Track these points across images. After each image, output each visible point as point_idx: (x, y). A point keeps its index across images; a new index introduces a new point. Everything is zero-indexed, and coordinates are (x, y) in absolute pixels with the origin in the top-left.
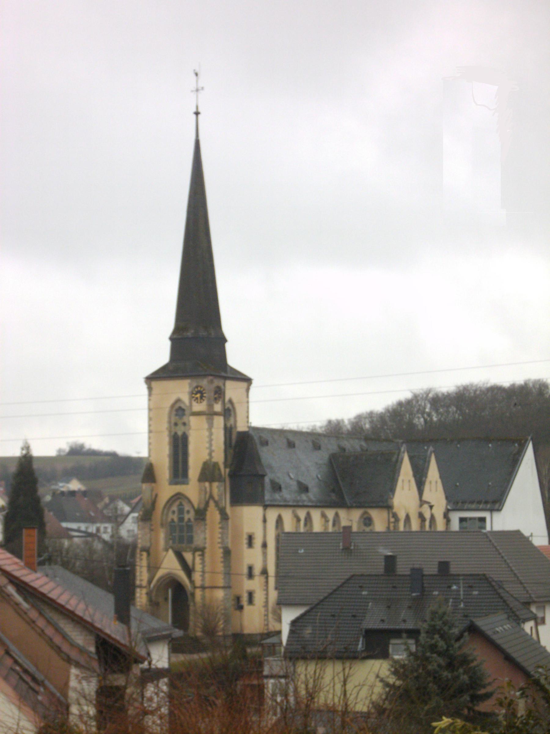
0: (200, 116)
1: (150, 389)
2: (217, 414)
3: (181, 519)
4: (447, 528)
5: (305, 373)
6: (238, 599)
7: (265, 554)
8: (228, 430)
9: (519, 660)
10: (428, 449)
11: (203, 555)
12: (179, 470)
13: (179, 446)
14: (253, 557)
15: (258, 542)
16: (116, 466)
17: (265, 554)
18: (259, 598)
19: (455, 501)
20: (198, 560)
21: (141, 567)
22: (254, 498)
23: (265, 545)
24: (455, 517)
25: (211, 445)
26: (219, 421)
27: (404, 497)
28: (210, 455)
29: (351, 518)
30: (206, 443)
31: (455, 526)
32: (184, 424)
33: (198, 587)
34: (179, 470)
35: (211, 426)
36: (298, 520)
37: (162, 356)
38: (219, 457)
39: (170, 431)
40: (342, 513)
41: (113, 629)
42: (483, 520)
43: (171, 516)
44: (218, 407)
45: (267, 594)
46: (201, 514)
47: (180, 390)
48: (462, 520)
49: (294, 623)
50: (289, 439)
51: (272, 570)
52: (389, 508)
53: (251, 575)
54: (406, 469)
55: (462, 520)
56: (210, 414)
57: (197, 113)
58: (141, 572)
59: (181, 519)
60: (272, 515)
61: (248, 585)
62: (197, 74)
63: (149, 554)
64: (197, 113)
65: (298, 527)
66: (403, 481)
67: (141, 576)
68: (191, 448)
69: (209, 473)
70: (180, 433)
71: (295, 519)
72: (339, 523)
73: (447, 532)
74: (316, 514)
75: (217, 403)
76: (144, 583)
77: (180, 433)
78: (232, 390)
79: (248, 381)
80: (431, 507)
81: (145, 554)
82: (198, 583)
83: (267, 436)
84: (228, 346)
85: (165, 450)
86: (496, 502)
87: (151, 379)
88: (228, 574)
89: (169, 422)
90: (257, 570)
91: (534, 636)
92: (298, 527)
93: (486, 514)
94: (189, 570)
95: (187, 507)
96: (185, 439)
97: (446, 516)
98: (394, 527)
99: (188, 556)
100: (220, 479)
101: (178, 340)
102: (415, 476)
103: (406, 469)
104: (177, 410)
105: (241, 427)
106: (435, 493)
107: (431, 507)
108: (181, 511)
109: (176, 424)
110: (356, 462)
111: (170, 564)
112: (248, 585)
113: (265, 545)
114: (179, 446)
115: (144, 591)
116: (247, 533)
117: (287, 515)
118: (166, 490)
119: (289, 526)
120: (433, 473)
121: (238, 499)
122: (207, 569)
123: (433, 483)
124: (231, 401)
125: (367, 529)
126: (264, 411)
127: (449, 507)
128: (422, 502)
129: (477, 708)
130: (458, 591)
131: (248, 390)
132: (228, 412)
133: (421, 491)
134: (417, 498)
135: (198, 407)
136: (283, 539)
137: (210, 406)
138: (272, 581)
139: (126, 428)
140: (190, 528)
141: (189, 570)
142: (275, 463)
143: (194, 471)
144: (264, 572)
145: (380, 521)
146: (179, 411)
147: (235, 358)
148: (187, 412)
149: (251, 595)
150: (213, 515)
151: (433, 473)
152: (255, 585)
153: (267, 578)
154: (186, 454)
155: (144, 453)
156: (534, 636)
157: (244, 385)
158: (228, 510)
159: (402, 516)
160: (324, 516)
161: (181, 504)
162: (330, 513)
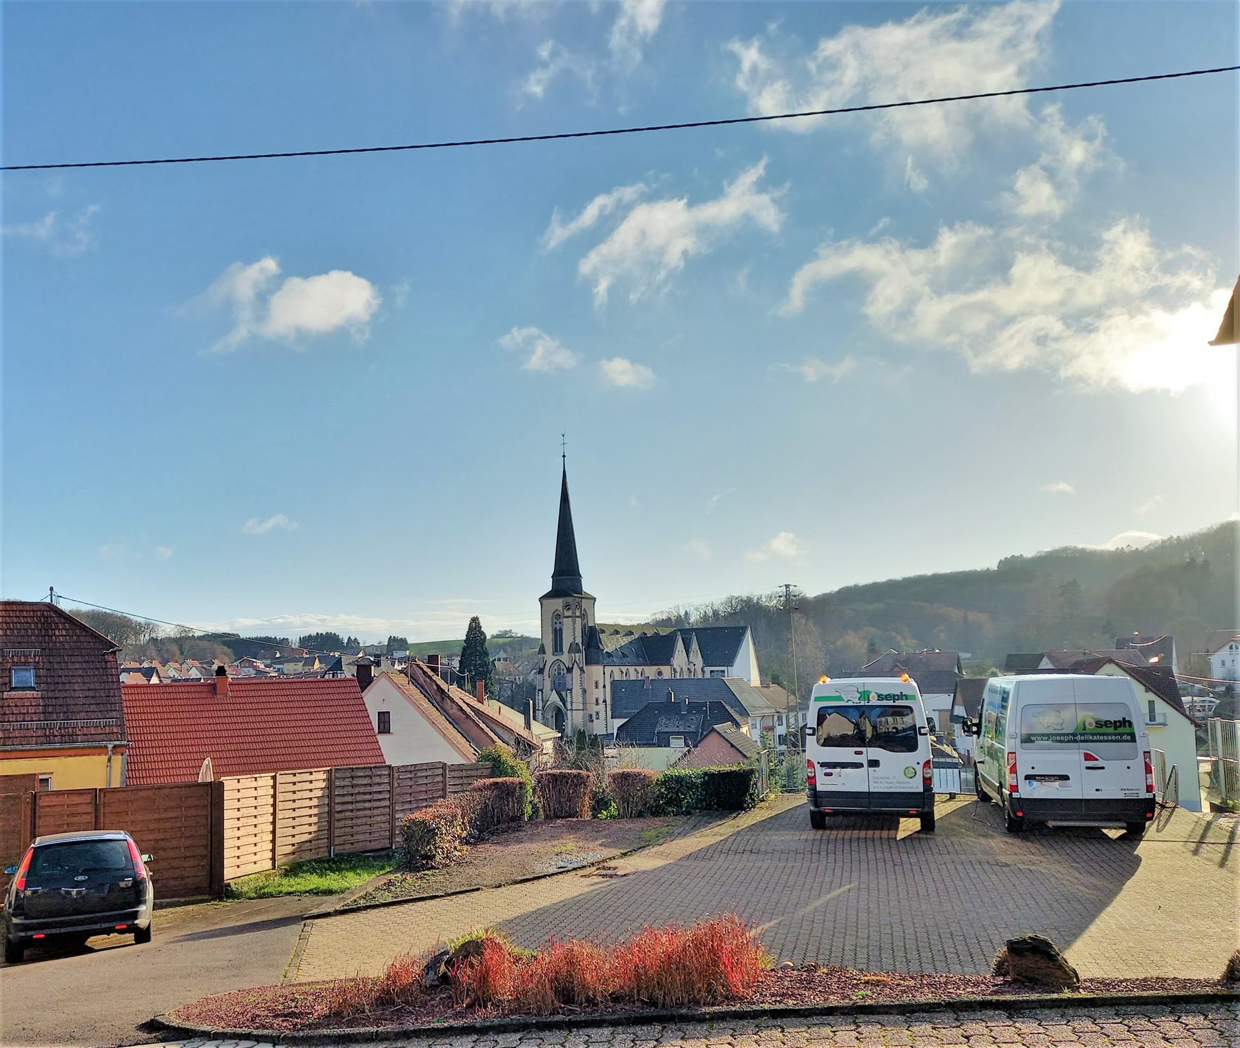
6: (591, 716)
8: (584, 627)
9: (453, 1040)
12: (558, 648)
13: (558, 634)
15: (601, 685)
18: (602, 715)
19: (707, 663)
24: (708, 669)
29: (651, 672)
30: (572, 633)
31: (708, 675)
34: (558, 648)
35: (574, 623)
37: (548, 587)
41: (525, 733)
44: (578, 613)
46: (570, 670)
47: (558, 603)
50: (616, 630)
51: (609, 702)
53: (597, 704)
54: (680, 645)
56: (574, 617)
60: (608, 669)
69: (574, 649)
74: (632, 669)
75: (748, 47)
78: (585, 603)
85: (550, 636)
86: (729, 661)
87: (541, 599)
99: (563, 694)
100: (579, 651)
103: (680, 645)
106: (698, 660)
111: (554, 698)
114: (558, 634)
120: (695, 646)
121: (589, 662)
126: (603, 615)
128: (690, 663)
132: (583, 616)
142: (610, 644)
143: (566, 648)
144: (605, 701)
145: (666, 671)
146: (557, 616)
150: (576, 671)
151: (695, 646)
162: (639, 669)
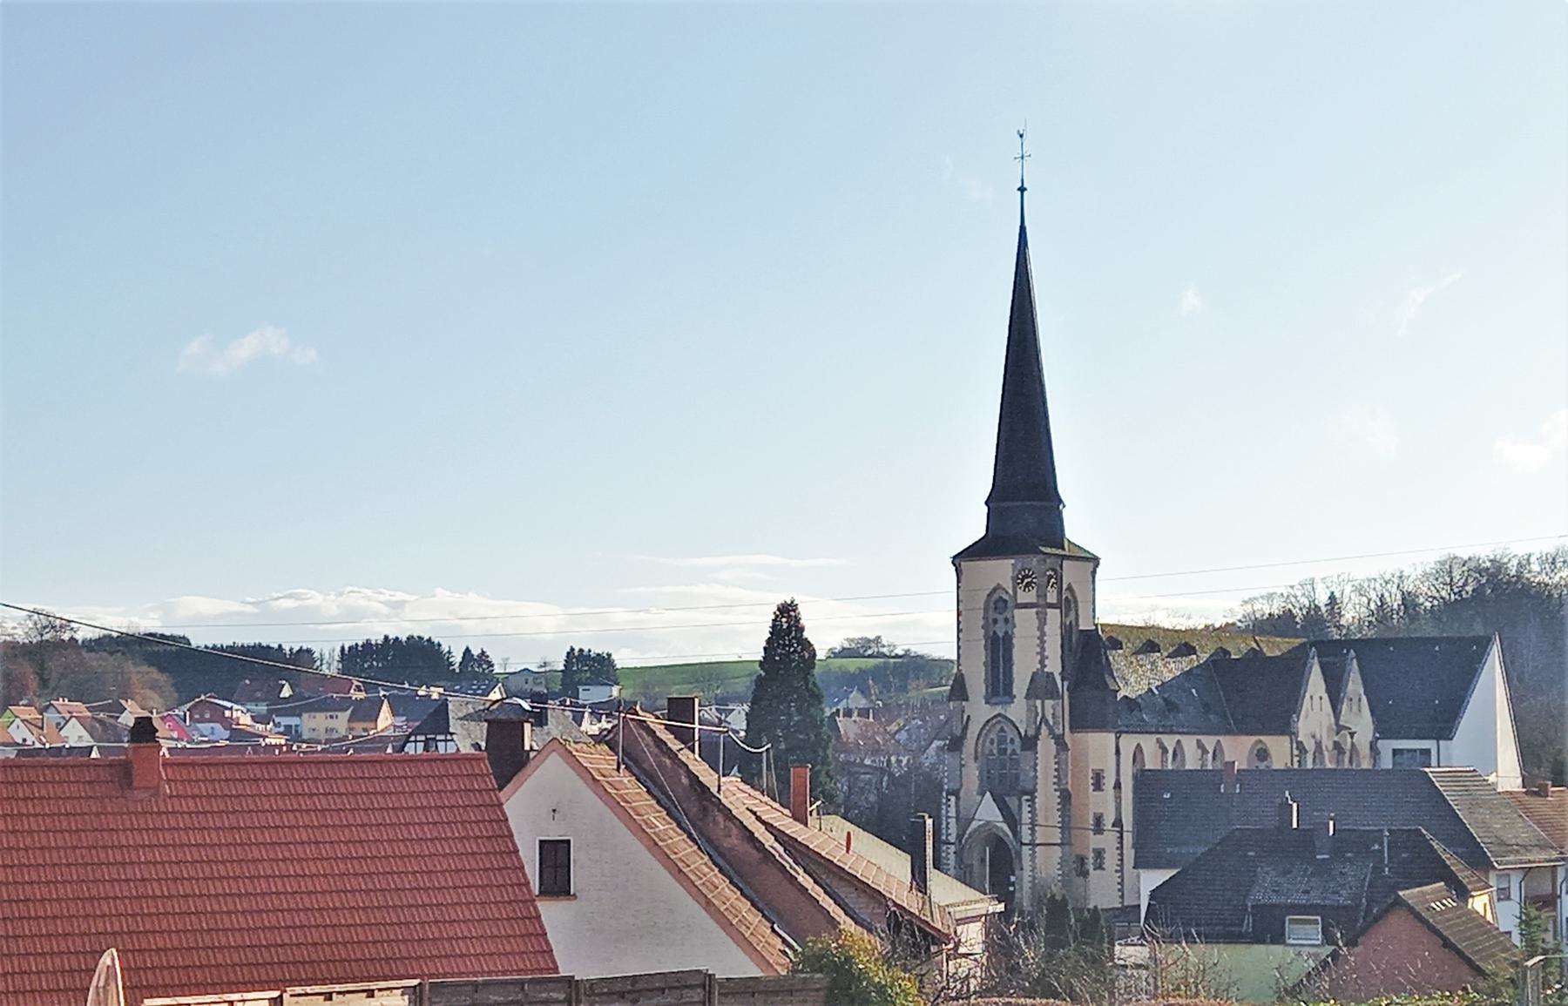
2: (1052, 606)
3: (1003, 751)
5: (1170, 556)
6: (1082, 860)
7: (1118, 798)
8: (1067, 631)
11: (1032, 800)
12: (999, 687)
14: (1103, 804)
15: (1109, 782)
16: (914, 667)
17: (1118, 798)
18: (1111, 860)
19: (1384, 728)
20: (1026, 808)
22: (1100, 726)
23: (1118, 786)
24: (1387, 746)
28: (1042, 662)
30: (1037, 648)
31: (1387, 762)
32: (1006, 620)
34: (999, 687)
35: (1042, 622)
36: (1165, 751)
37: (975, 528)
38: (1054, 666)
42: (1427, 752)
44: (1052, 597)
46: (1030, 743)
47: (1001, 571)
48: (1396, 752)
49: (1154, 894)
51: (1128, 823)
52: (1293, 734)
53: (1098, 827)
54: (1316, 683)
55: (1396, 752)
56: (1041, 606)
57: (1022, 190)
59: (1003, 751)
60: (1129, 743)
61: (1095, 841)
64: (1022, 190)
65: (1164, 761)
68: (1016, 654)
69: (1041, 686)
73: (1375, 772)
74: (1189, 743)
76: (952, 839)
79: (1095, 561)
80: (1352, 735)
81: (953, 798)
82: (1026, 839)
83: (1114, 638)
84: (1067, 514)
87: (958, 559)
88: (1066, 827)
92: (1164, 761)
94: (1012, 821)
95: (1011, 734)
96: (1008, 640)
97: (1373, 747)
99: (1012, 802)
102: (1328, 691)
103: (1316, 683)
107: (1352, 735)
108: (1002, 741)
109: (995, 621)
110: (1246, 675)
111: (988, 811)
112: (1095, 841)
113: (1118, 786)
114: (999, 650)
117: (1149, 743)
118: (979, 711)
119: (1151, 763)
120: (1354, 684)
121: (1081, 721)
122: (1040, 820)
123: (1355, 700)
124: (1070, 588)
125: (1262, 766)
126: (1117, 602)
128: (1340, 728)
129: (539, 904)
130: (1381, 851)
131: (1094, 573)
132: (1068, 604)
133: (1336, 712)
134: (1328, 721)
135: (1025, 597)
136: (1144, 779)
137: (1042, 595)
138: (1128, 839)
139: (929, 624)
141: (1012, 821)
143: (1020, 686)
144: (1118, 823)
145: (1280, 751)
146: (998, 605)
148: (1010, 604)
149: (1099, 854)
150: (1046, 746)
151: (1354, 684)
154: (1009, 661)
157: (1091, 565)
158: (1067, 738)
159: (1310, 746)
160: (1200, 745)
161: (1002, 730)
162: (1209, 742)
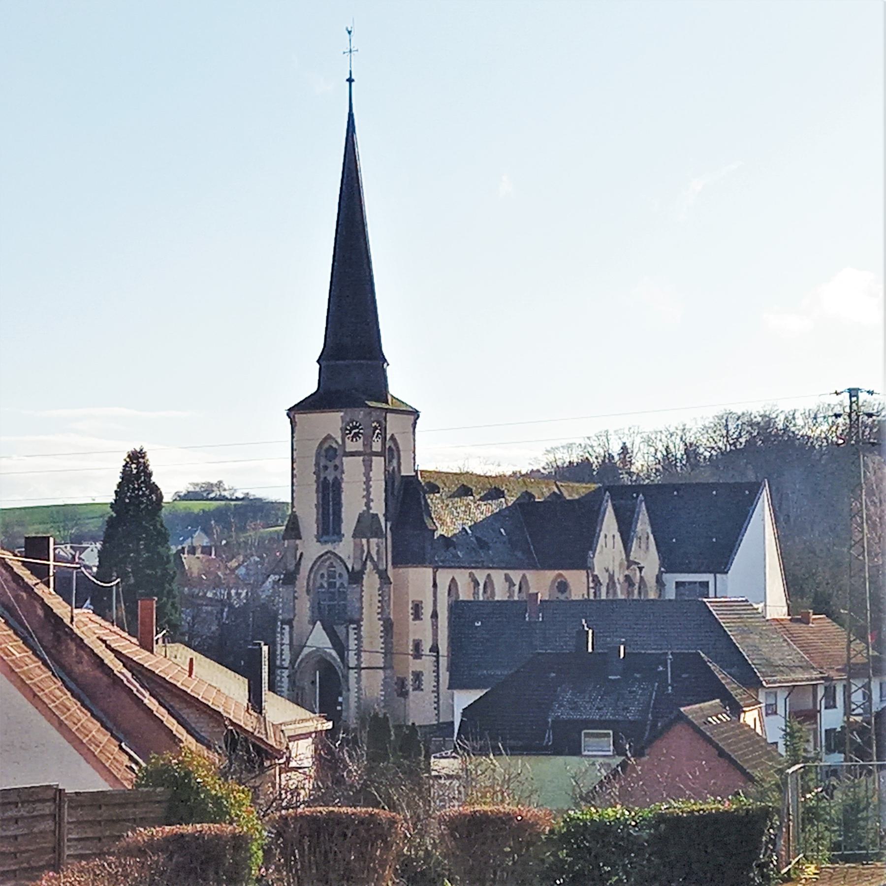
0: (353, 84)
1: (293, 423)
2: (377, 454)
3: (332, 585)
4: (660, 596)
6: (402, 682)
7: (435, 627)
8: (390, 478)
10: (638, 496)
12: (329, 526)
13: (329, 494)
14: (421, 631)
15: (427, 611)
17: (435, 627)
18: (428, 681)
21: (282, 645)
24: (671, 579)
25: (369, 493)
26: (378, 463)
27: (608, 552)
28: (367, 505)
30: (363, 492)
32: (336, 467)
33: (352, 668)
34: (329, 526)
36: (477, 584)
37: (307, 383)
38: (378, 508)
39: (318, 477)
40: (530, 575)
43: (319, 581)
44: (377, 446)
45: (438, 676)
46: (356, 577)
47: (331, 422)
53: (418, 653)
54: (609, 524)
57: (350, 80)
58: (282, 650)
59: (332, 585)
60: (444, 577)
61: (415, 665)
62: (349, 32)
63: (291, 627)
65: (476, 593)
66: (606, 536)
67: (282, 654)
69: (367, 526)
70: (330, 479)
71: (472, 584)
72: (528, 588)
74: (498, 576)
76: (286, 664)
77: (330, 479)
78: (393, 424)
79: (415, 414)
80: (641, 569)
81: (287, 627)
86: (720, 561)
87: (292, 412)
89: (317, 464)
90: (426, 647)
91: (758, 730)
92: (476, 593)
93: (708, 577)
94: (340, 647)
96: (337, 486)
97: (659, 580)
98: (595, 593)
100: (378, 533)
101: (328, 359)
103: (609, 524)
104: (327, 450)
105: (406, 471)
107: (641, 569)
108: (332, 575)
109: (326, 468)
110: (549, 517)
111: (319, 639)
112: (415, 665)
113: (435, 615)
114: (329, 494)
115: (286, 673)
116: (414, 640)
117: (462, 577)
119: (465, 594)
120: (643, 525)
125: (562, 597)
126: (434, 451)
127: (662, 569)
128: (630, 563)
132: (391, 452)
135: (351, 446)
136: (457, 609)
137: (368, 444)
138: (444, 662)
139: (266, 470)
140: (343, 595)
143: (348, 525)
144: (435, 649)
145: (578, 584)
147: (399, 385)
148: (339, 452)
149: (418, 676)
150: (371, 580)
151: (643, 525)
152: (425, 664)
153: (437, 657)
154: (338, 504)
155: (285, 496)
156: (758, 730)
158: (390, 573)
159: (604, 579)
160: (507, 578)
162: (516, 576)
